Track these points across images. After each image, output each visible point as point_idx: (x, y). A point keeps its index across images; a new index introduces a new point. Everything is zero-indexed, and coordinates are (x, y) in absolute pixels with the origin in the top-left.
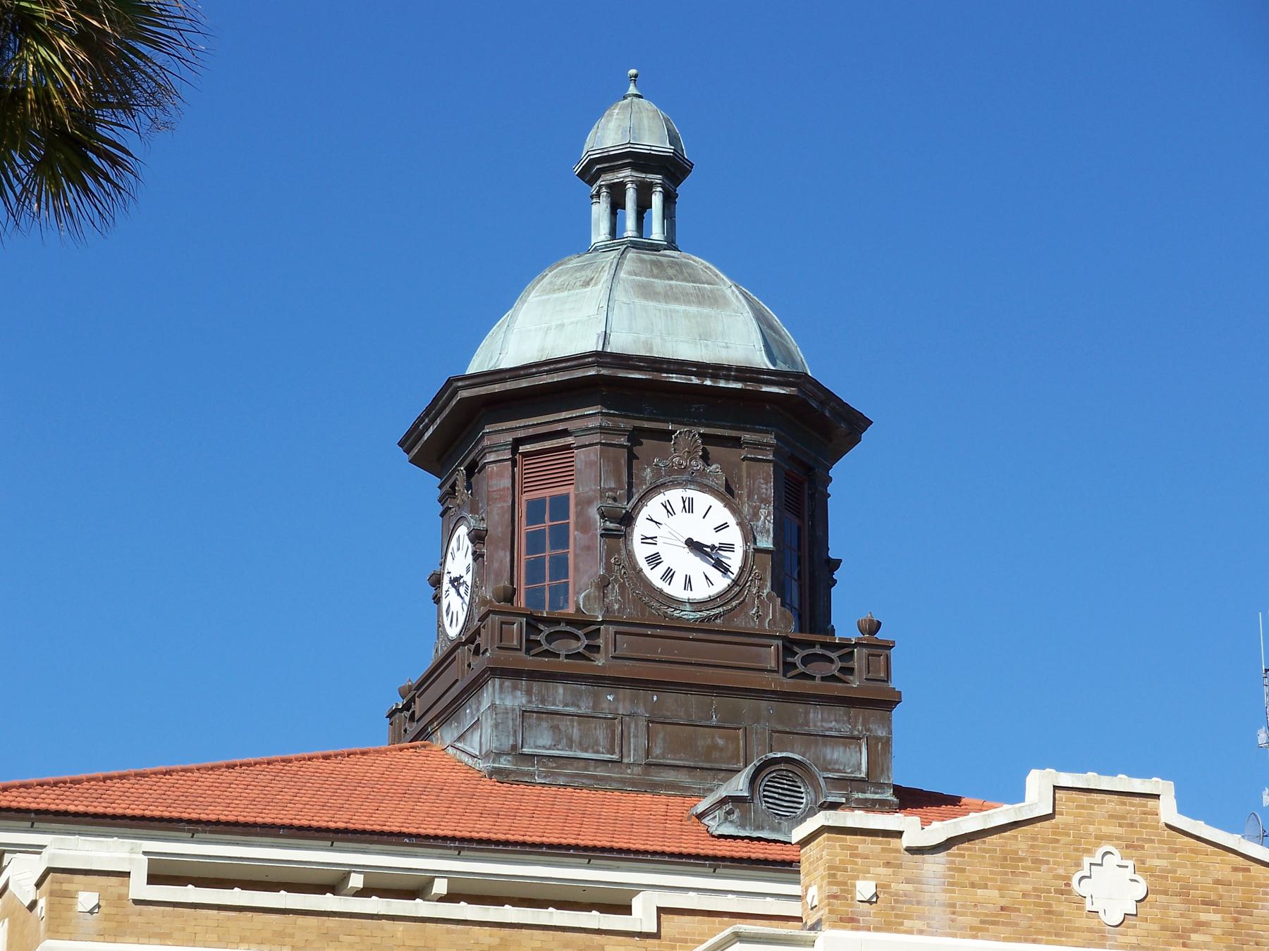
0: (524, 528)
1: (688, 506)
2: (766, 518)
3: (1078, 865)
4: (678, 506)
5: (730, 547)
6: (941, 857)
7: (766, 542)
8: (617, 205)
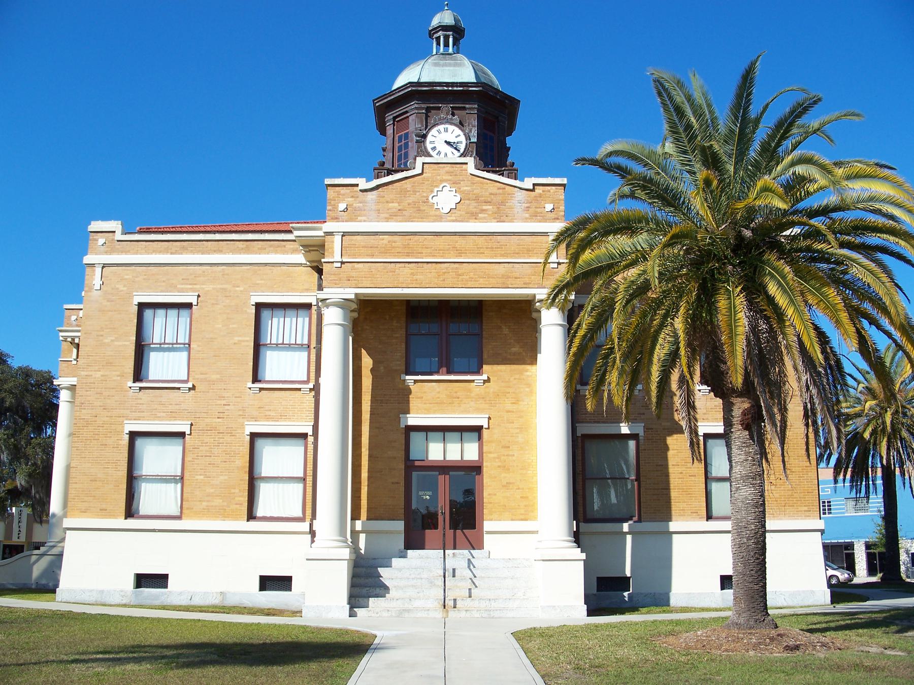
0: (397, 145)
1: (446, 130)
2: (474, 132)
3: (432, 191)
4: (442, 130)
5: (461, 142)
6: (375, 192)
7: (474, 140)
8: (438, 44)
